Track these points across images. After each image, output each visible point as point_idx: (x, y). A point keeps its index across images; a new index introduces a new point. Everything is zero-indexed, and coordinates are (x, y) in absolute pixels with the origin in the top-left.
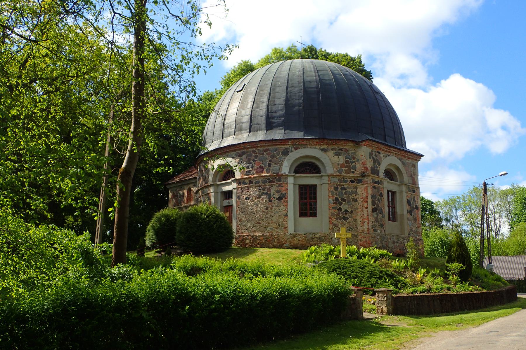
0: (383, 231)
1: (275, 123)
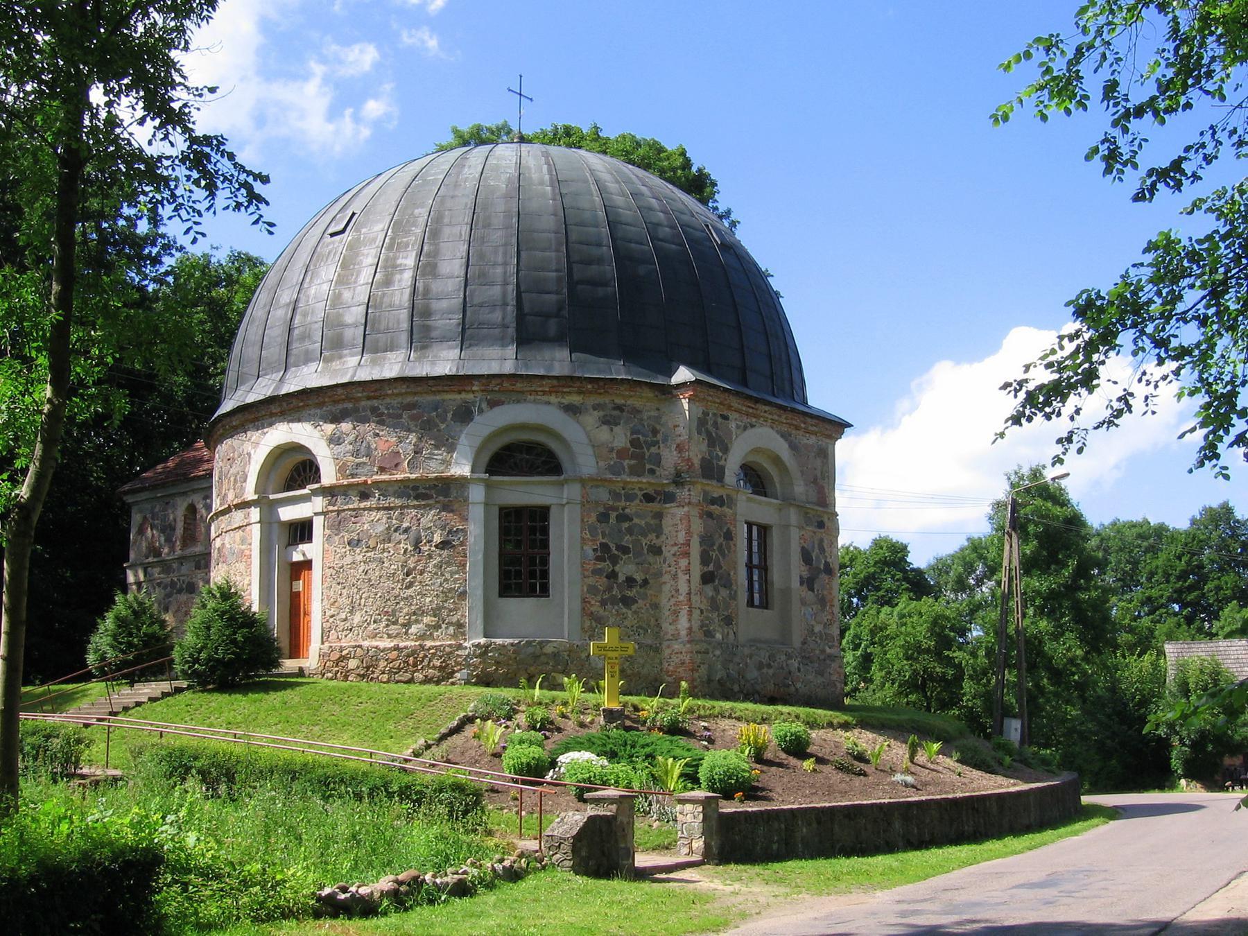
0: (732, 636)
1: (436, 328)
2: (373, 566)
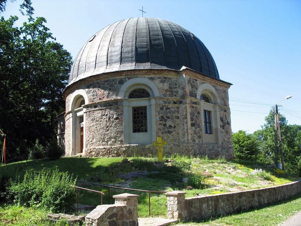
0: (201, 141)
1: (113, 60)
2: (98, 126)
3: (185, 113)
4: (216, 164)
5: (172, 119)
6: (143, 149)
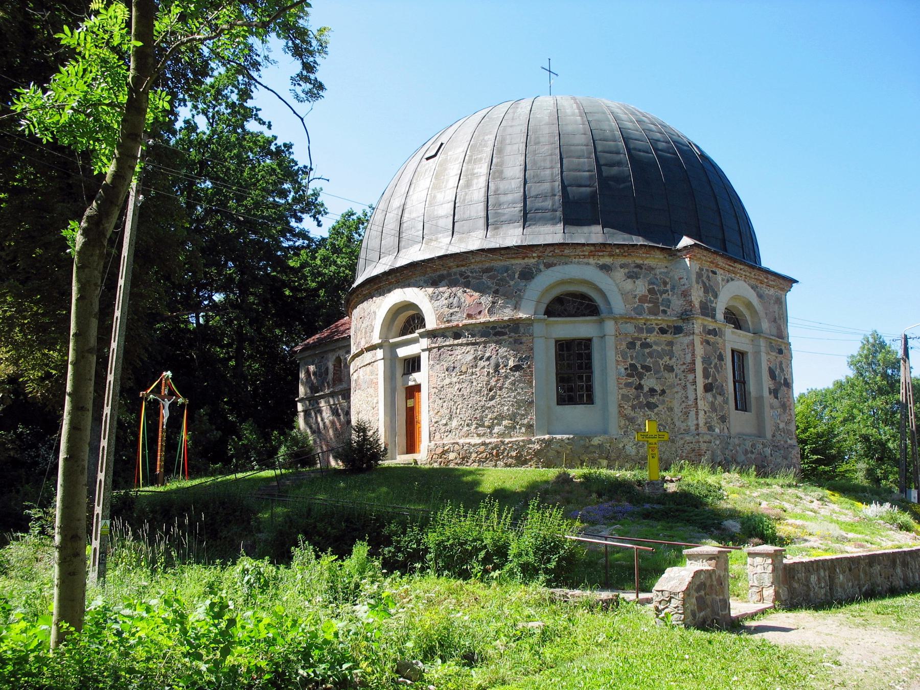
0: (726, 430)
1: (504, 214)
2: (464, 385)
3: (689, 359)
4: (777, 489)
5: (657, 372)
6: (587, 449)
